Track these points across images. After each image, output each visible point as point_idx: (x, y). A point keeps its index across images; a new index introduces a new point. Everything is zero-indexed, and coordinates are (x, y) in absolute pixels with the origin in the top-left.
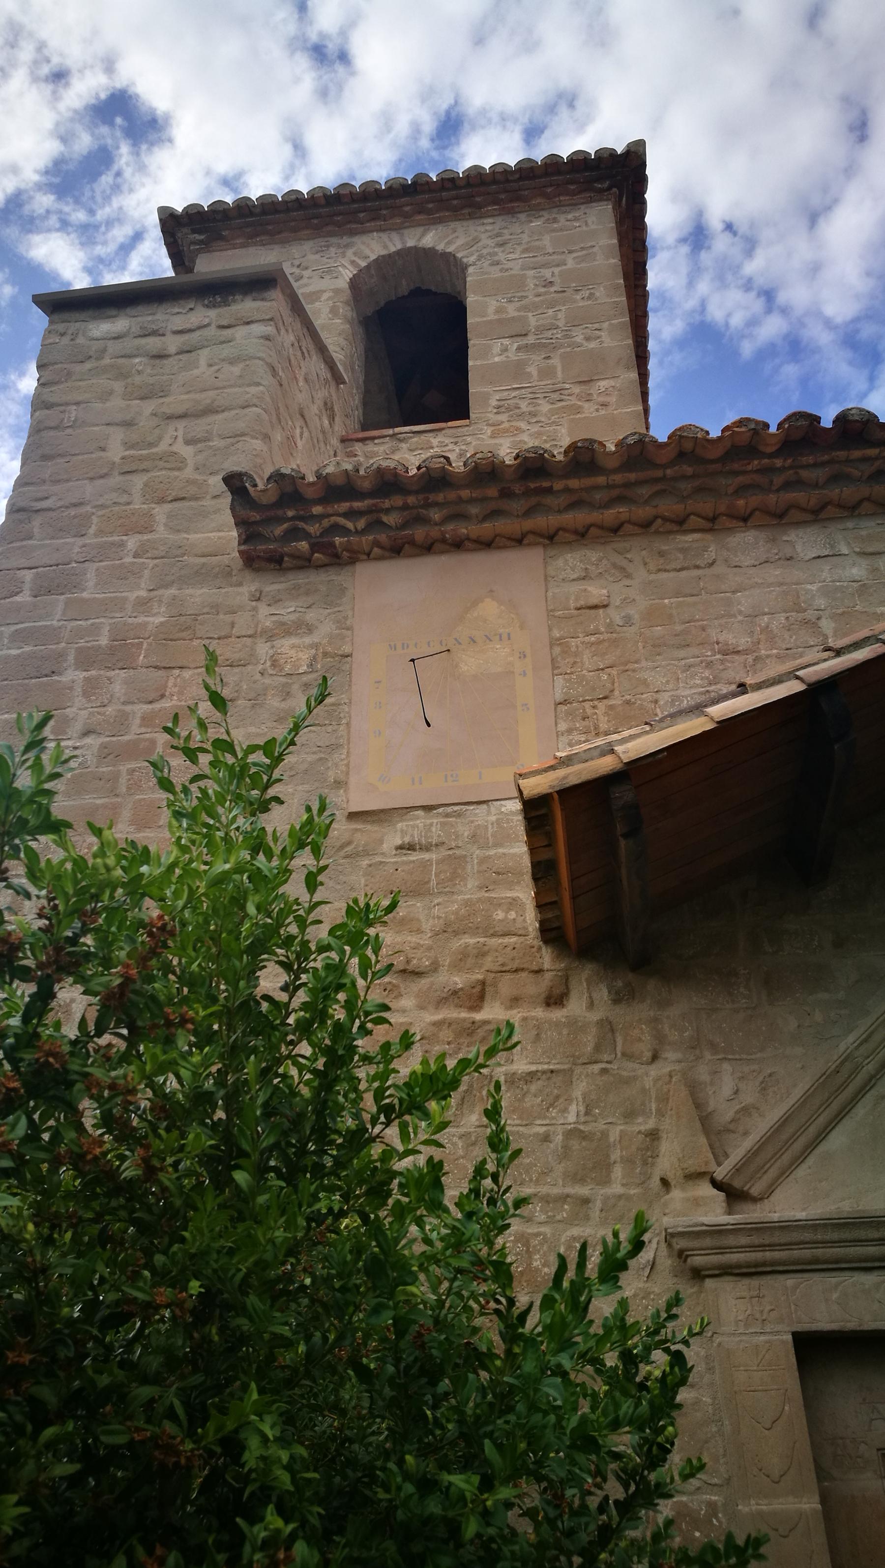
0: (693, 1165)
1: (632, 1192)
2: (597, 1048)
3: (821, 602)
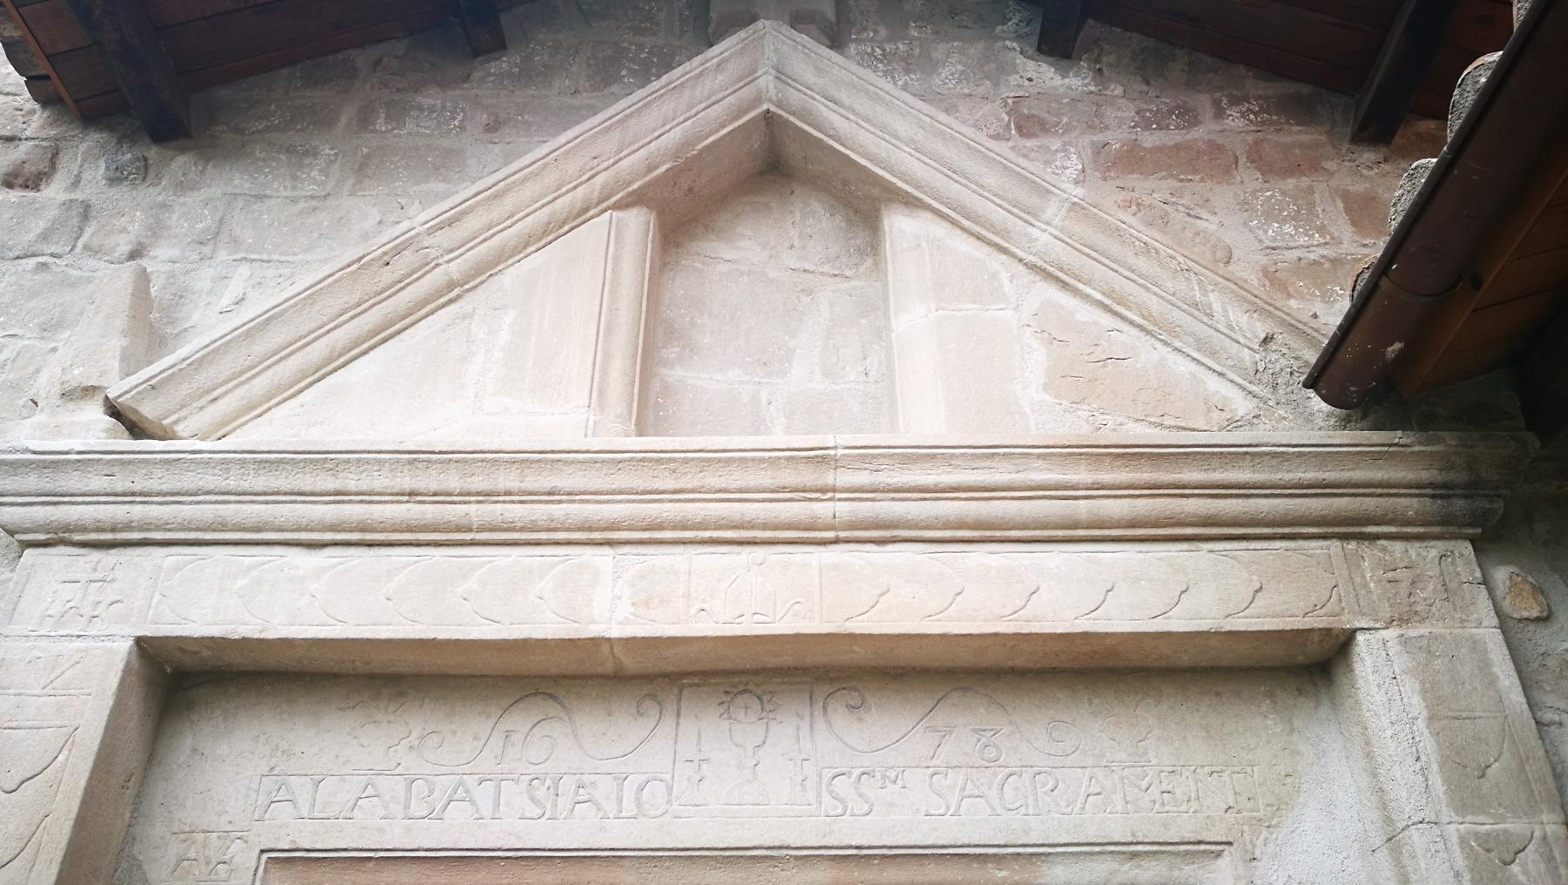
2: (45, 237)
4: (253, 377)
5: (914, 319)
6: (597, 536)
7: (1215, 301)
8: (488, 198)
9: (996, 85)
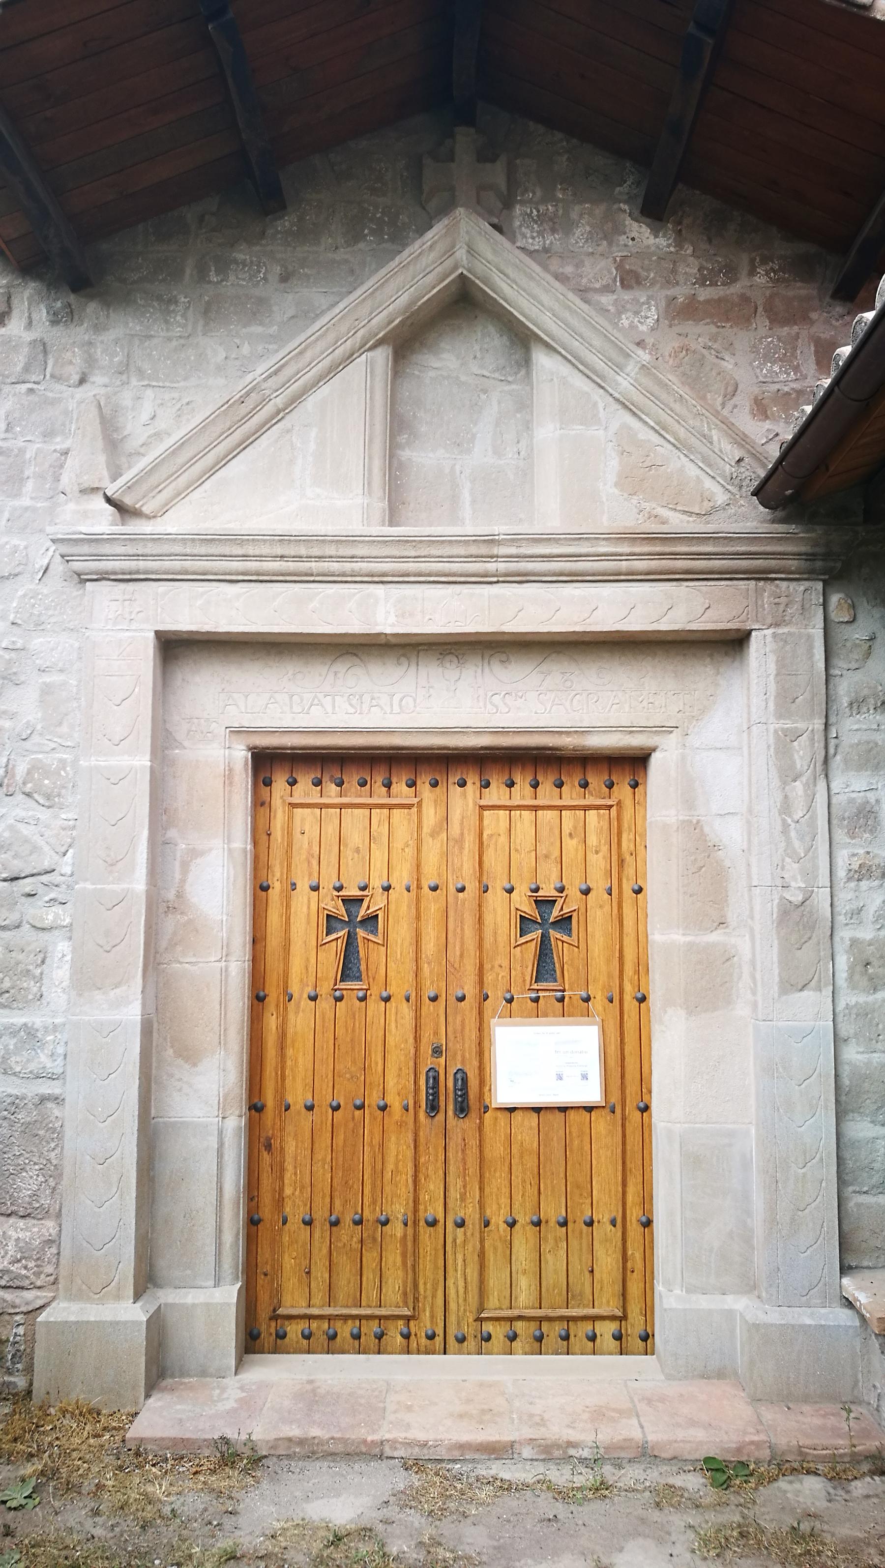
0: (88, 481)
1: (39, 505)
2: (27, 369)
4: (178, 477)
5: (546, 432)
6: (376, 579)
7: (715, 435)
8: (296, 355)
9: (610, 244)
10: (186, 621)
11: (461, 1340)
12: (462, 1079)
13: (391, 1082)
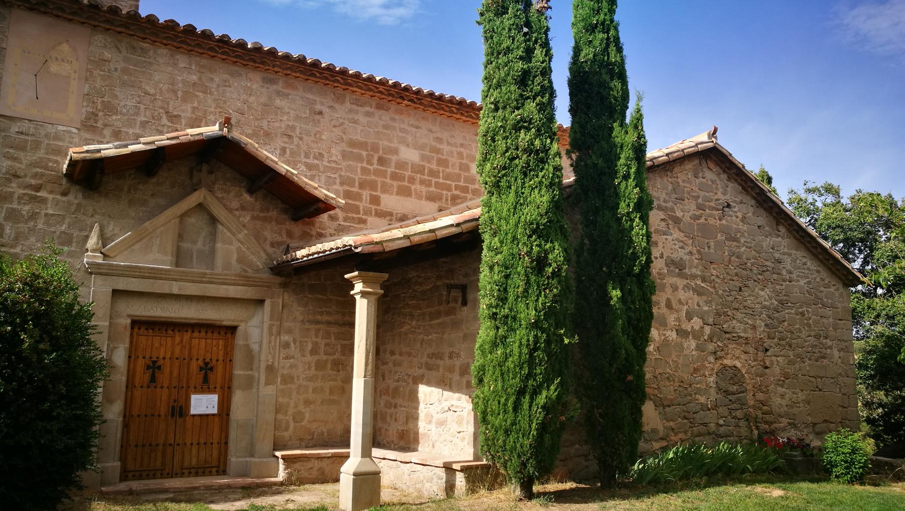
3: (180, 85)
10: (121, 287)
11: (177, 474)
12: (181, 407)
13: (162, 409)
